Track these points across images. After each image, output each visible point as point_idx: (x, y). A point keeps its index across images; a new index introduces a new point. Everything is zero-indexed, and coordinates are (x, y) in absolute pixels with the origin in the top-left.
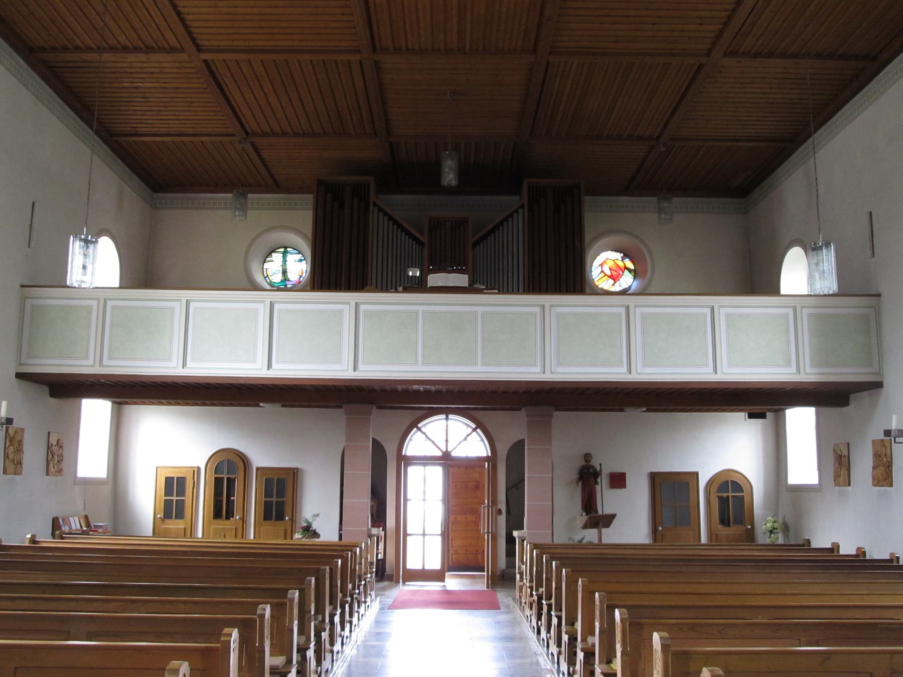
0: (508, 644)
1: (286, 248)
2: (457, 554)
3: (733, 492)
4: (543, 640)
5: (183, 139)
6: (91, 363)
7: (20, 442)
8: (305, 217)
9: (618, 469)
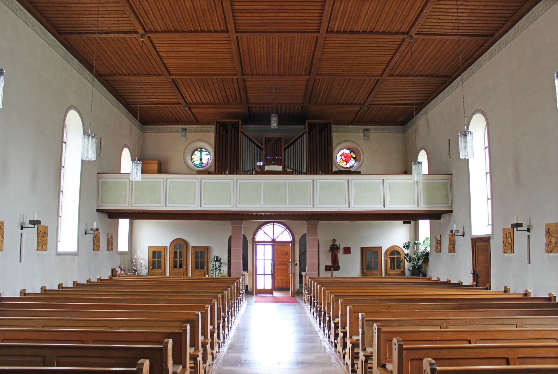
0: (306, 344)
1: (201, 149)
2: (278, 283)
3: (396, 255)
4: (326, 334)
5: (159, 105)
6: (127, 205)
8: (212, 136)
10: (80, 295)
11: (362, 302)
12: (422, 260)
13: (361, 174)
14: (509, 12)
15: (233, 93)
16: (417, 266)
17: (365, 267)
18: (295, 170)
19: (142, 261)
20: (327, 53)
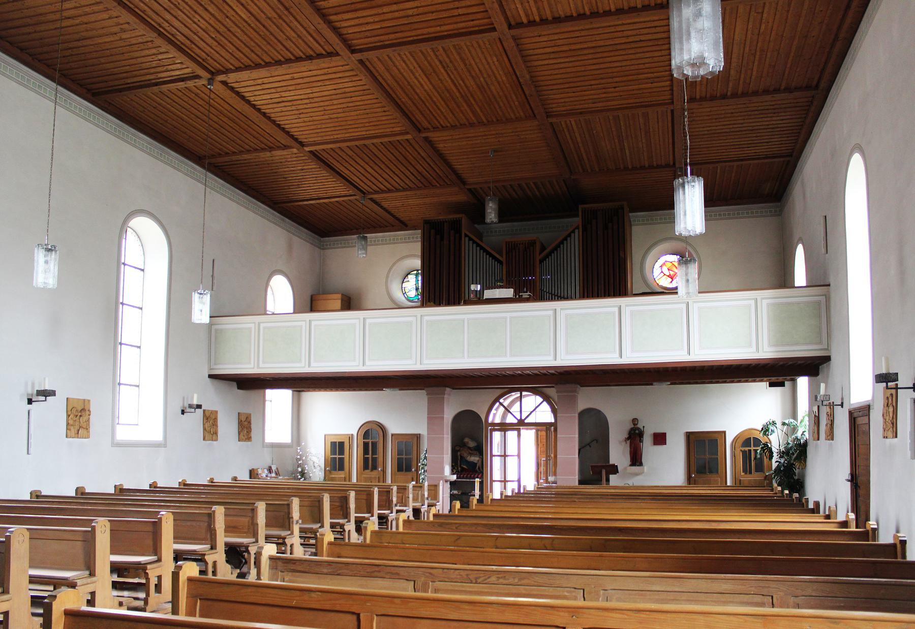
7: (215, 420)
9: (660, 430)
11: (454, 528)
17: (693, 468)
18: (554, 294)
19: (315, 459)
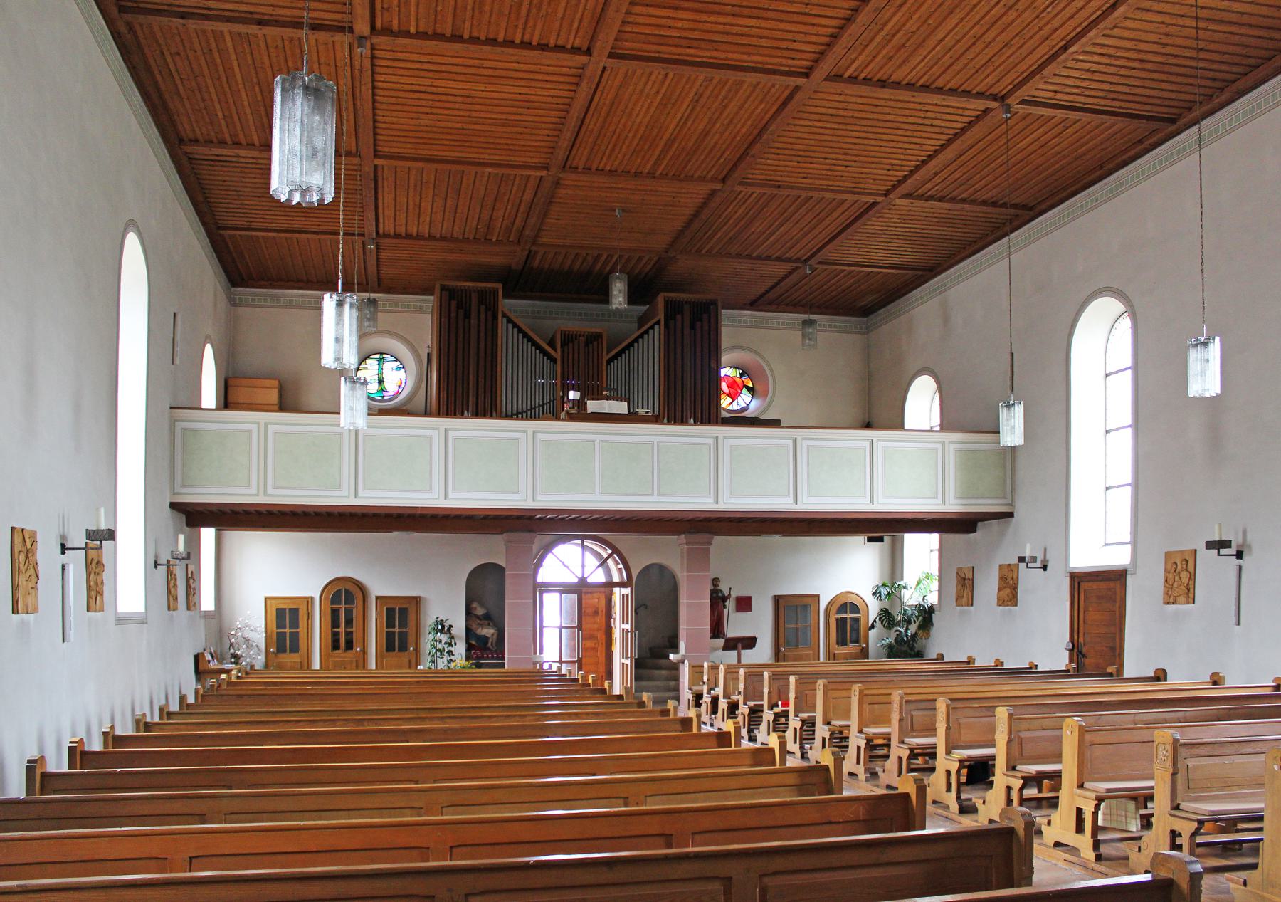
1: (381, 354)
9: (744, 593)
10: (302, 724)
12: (917, 623)
13: (782, 425)
14: (1235, 69)
15: (510, 213)
16: (907, 636)
20: (797, 129)
